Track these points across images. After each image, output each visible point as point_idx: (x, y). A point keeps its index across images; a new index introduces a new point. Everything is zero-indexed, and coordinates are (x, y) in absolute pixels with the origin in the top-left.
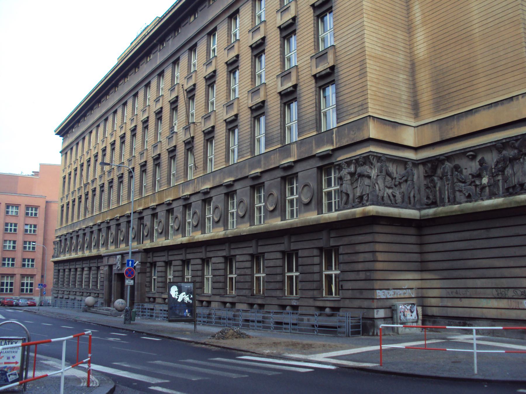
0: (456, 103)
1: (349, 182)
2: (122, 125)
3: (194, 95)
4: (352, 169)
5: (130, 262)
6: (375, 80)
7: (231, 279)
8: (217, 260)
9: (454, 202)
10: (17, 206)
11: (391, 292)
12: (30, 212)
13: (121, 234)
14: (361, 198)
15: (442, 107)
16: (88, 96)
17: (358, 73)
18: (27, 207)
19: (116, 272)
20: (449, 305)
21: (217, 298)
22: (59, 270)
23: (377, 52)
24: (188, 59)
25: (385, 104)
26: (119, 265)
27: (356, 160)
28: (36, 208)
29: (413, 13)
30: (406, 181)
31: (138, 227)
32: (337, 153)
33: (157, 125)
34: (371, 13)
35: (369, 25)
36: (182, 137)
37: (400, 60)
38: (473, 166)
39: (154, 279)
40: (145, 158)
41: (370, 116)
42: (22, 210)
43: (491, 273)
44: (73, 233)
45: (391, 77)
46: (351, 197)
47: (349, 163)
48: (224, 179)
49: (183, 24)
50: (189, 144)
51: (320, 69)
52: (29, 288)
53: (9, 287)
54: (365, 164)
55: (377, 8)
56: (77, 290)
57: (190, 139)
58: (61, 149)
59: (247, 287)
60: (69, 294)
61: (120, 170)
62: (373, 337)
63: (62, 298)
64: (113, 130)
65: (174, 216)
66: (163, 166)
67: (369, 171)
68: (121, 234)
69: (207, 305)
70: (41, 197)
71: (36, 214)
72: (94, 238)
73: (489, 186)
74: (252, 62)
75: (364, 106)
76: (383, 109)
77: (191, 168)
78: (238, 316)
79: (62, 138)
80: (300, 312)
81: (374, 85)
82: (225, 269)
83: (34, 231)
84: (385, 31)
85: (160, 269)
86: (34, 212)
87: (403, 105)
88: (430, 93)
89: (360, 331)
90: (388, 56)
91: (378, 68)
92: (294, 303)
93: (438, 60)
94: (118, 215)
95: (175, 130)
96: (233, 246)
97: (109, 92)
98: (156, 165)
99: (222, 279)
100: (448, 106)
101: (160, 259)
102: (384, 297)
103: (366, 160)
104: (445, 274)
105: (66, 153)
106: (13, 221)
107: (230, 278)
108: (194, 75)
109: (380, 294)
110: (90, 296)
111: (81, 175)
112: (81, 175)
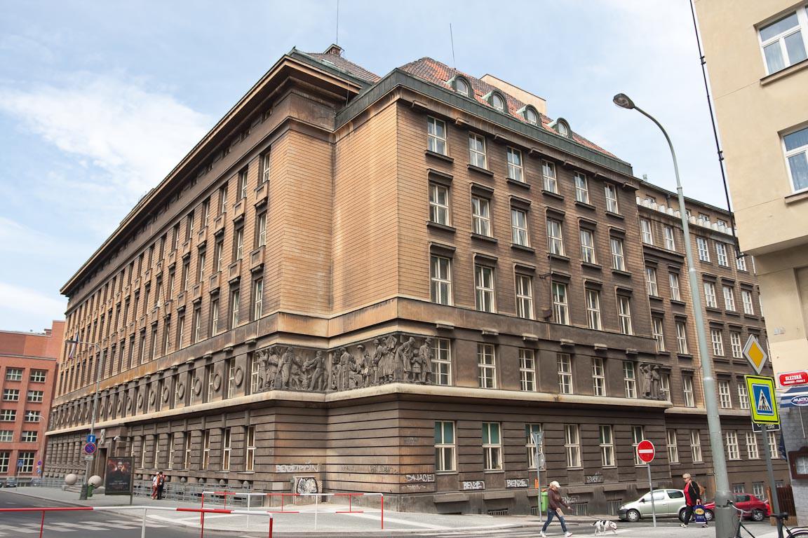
0: (356, 301)
1: (264, 369)
2: (201, 230)
3: (243, 227)
4: (265, 358)
5: (92, 438)
6: (290, 279)
7: (251, 452)
8: (215, 435)
9: (348, 387)
10: (21, 370)
11: (292, 467)
12: (36, 376)
13: (179, 389)
14: (269, 382)
15: (348, 303)
16: (170, 175)
17: (276, 273)
18: (33, 371)
19: (100, 447)
20: (343, 479)
21: (236, 476)
22: (53, 445)
23: (294, 254)
24: (219, 199)
25: (298, 300)
26: (102, 440)
27: (268, 349)
28: (44, 372)
29: (336, 217)
30: (315, 368)
31: (172, 387)
32: (259, 343)
33: (235, 239)
34: (292, 220)
35: (289, 230)
36: (227, 276)
37: (320, 259)
38: (359, 359)
39: (227, 452)
40: (238, 271)
41: (280, 312)
42: (25, 376)
43: (369, 451)
44: (81, 400)
45: (307, 275)
46: (264, 381)
47: (264, 352)
48: (188, 357)
49: (276, 104)
50: (235, 285)
51: (254, 265)
52: (28, 466)
53: (28, 466)
54: (274, 353)
55: (299, 214)
56: (56, 467)
57: (259, 267)
58: (66, 311)
59: (238, 462)
60: (54, 471)
61: (235, 272)
62: (603, 533)
63: (52, 477)
64: (150, 269)
65: (236, 368)
66: (223, 299)
67: (277, 360)
68: (179, 389)
69: (248, 486)
70: (50, 360)
71: (43, 379)
72: (140, 396)
73: (369, 376)
74: (215, 249)
75: (277, 302)
76: (296, 305)
77: (259, 307)
78: (189, 490)
79: (68, 298)
80: (255, 487)
81: (289, 284)
82: (222, 442)
83: (40, 399)
84: (307, 234)
85: (148, 443)
86: (40, 377)
87: (319, 300)
88: (341, 290)
89: (252, 497)
90: (307, 256)
91: (294, 269)
92: (225, 477)
93: (348, 261)
94: (108, 387)
95: (158, 305)
96: (159, 426)
97: (146, 223)
98: (197, 310)
99: (240, 452)
100: (351, 302)
101: (137, 434)
102: (285, 472)
103: (276, 350)
104: (341, 451)
105: (70, 316)
106: (15, 387)
107: (249, 451)
108: (266, 186)
109: (280, 469)
110: (71, 473)
111: (135, 307)
112: (135, 307)
